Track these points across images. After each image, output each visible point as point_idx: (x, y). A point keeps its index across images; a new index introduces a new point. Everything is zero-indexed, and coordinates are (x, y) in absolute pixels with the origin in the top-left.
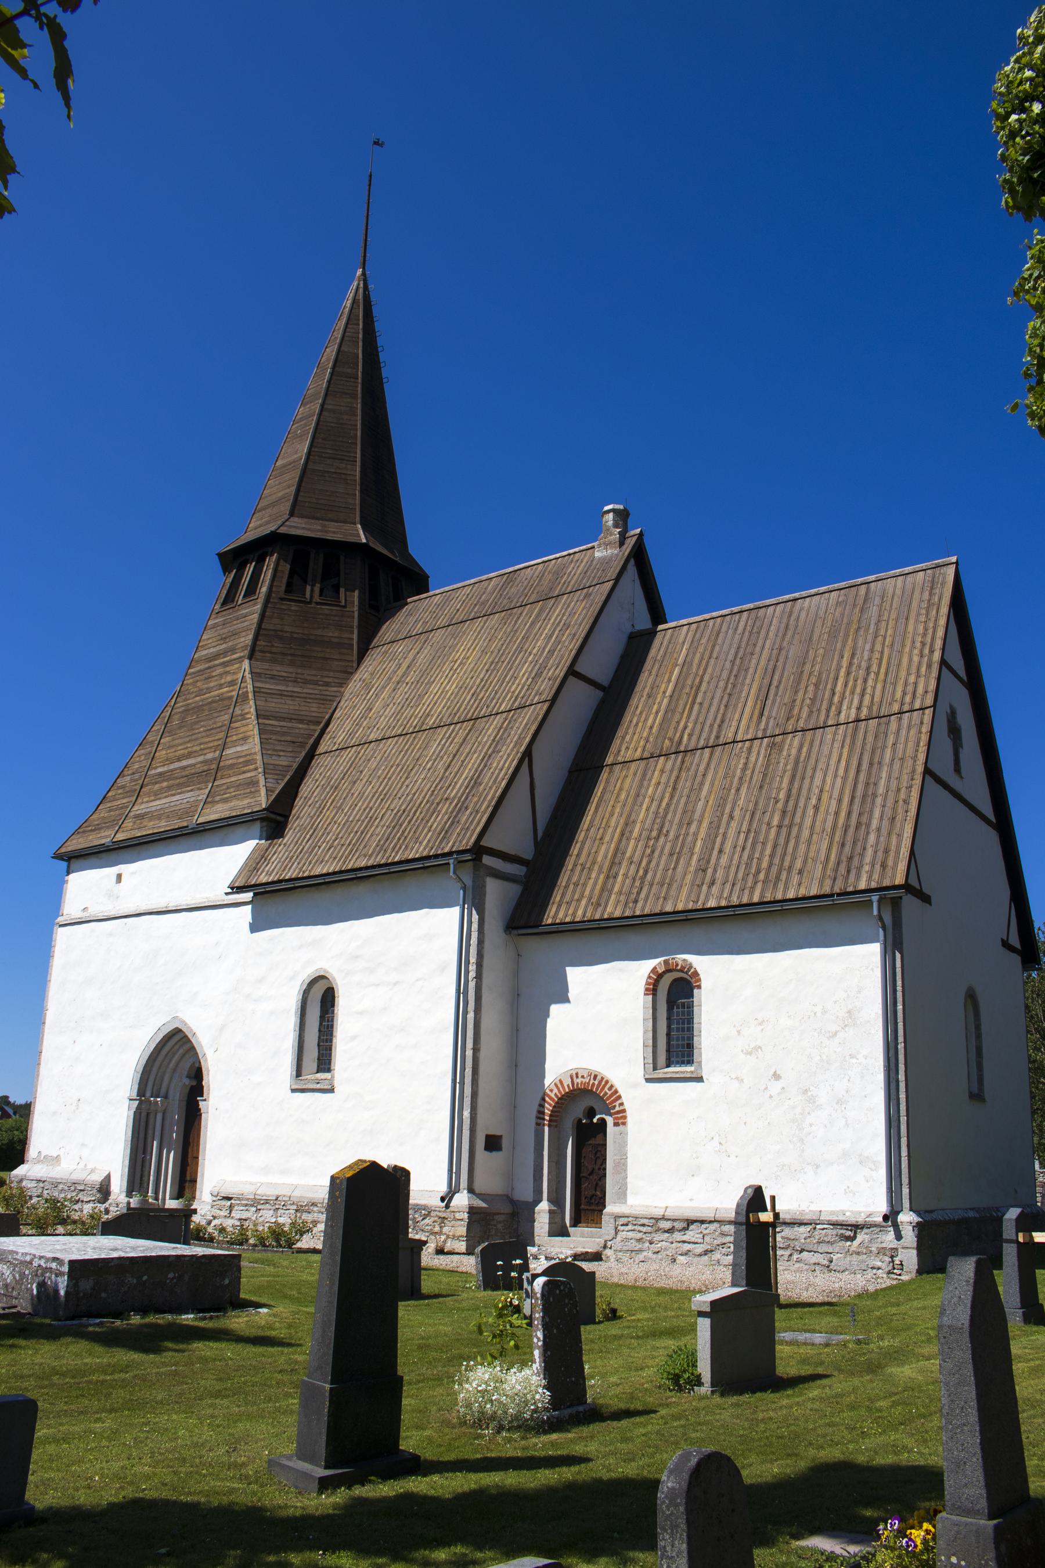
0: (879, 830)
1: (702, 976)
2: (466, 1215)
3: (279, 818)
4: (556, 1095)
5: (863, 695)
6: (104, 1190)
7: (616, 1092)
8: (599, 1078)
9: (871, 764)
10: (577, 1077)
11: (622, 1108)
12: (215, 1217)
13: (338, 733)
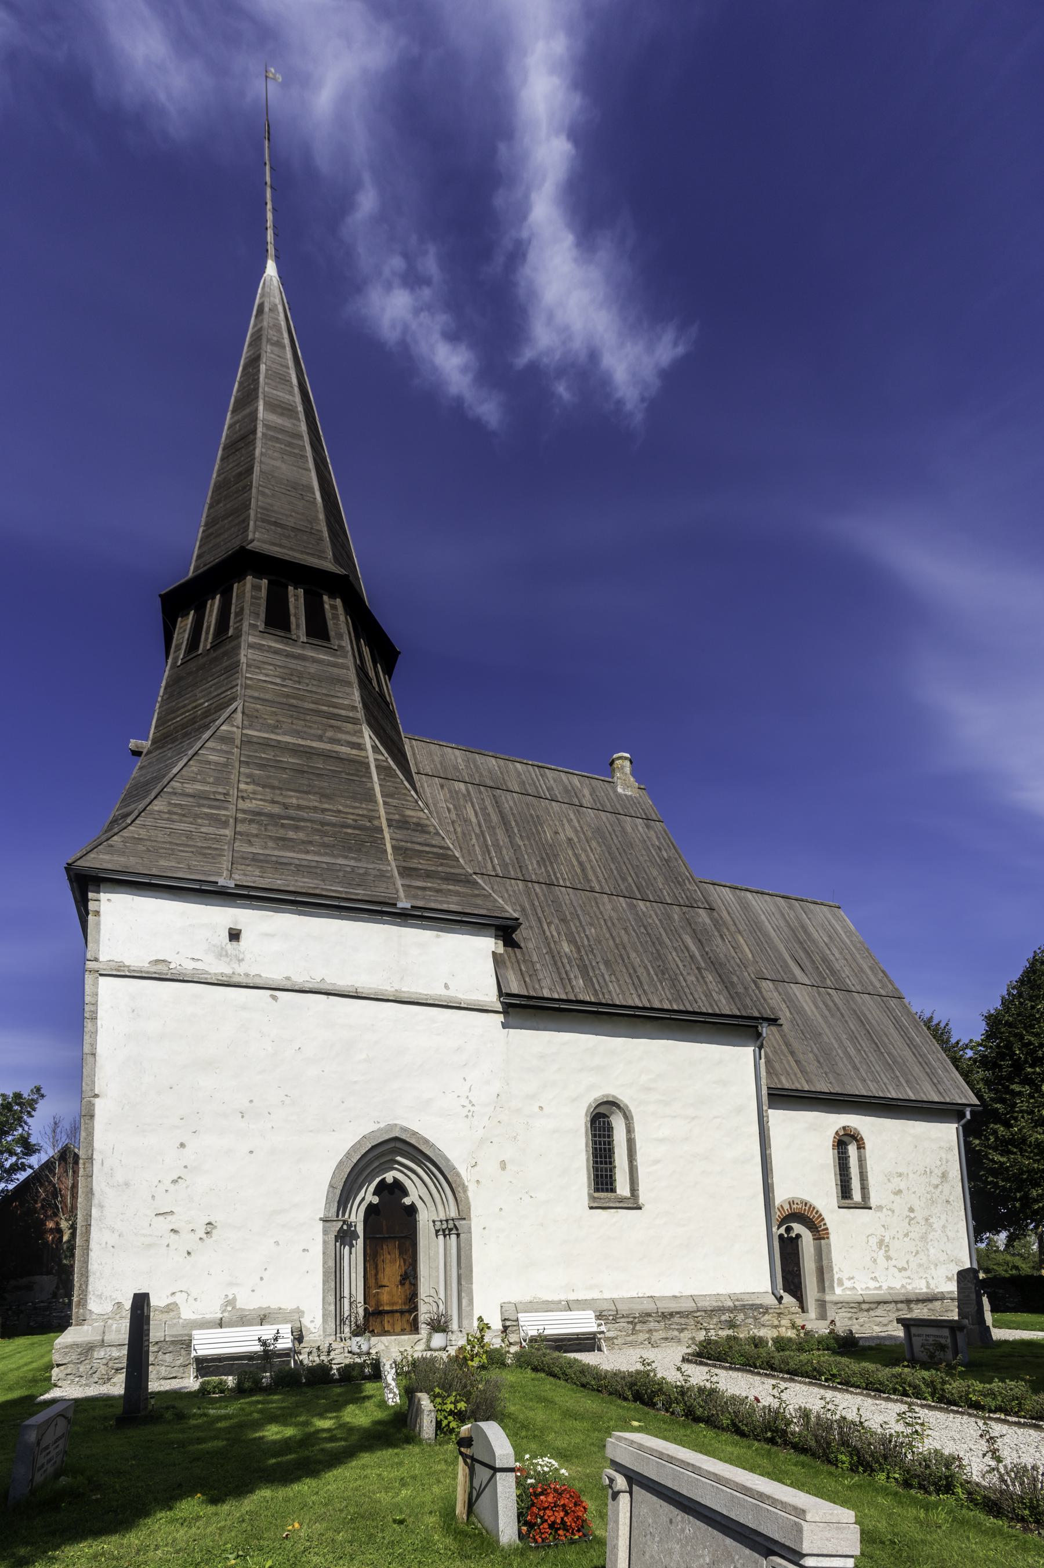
1: (866, 1141)
7: (821, 1215)
8: (808, 1205)
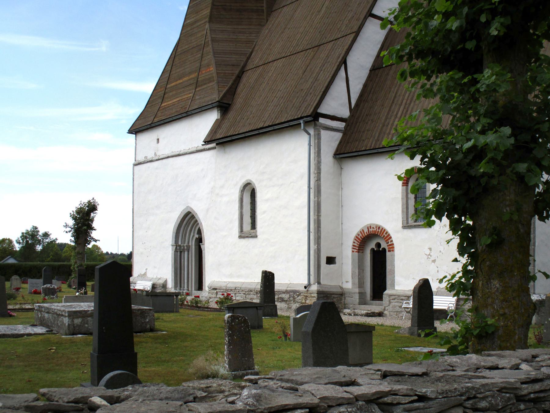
2: (316, 295)
3: (226, 105)
4: (361, 237)
6: (164, 286)
7: (389, 235)
8: (381, 228)
10: (370, 228)
11: (392, 243)
12: (210, 298)
13: (256, 60)
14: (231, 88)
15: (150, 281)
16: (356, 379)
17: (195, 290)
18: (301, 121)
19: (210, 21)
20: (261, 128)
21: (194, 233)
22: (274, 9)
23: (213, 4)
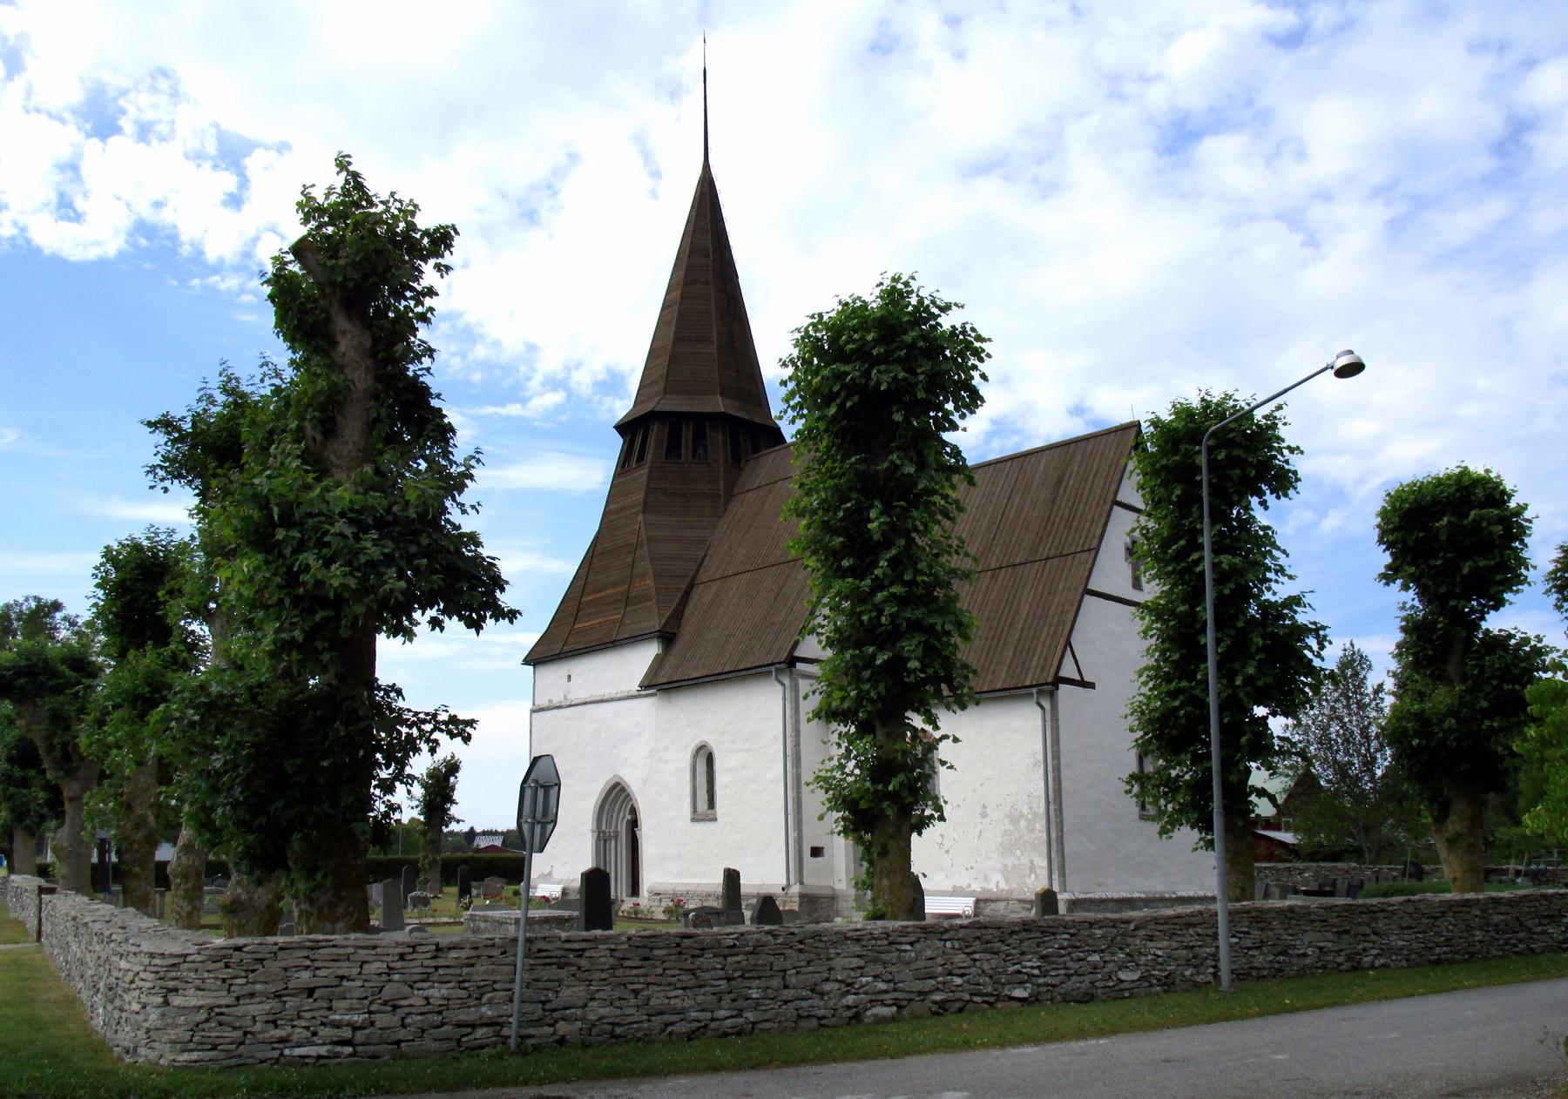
0: (1044, 643)
5: (1054, 538)
9: (1049, 592)
13: (711, 569)
14: (676, 609)
15: (559, 883)
16: (442, 631)
17: (627, 896)
18: (773, 668)
19: (644, 511)
20: (719, 674)
21: (625, 813)
22: (735, 492)
23: (648, 486)
